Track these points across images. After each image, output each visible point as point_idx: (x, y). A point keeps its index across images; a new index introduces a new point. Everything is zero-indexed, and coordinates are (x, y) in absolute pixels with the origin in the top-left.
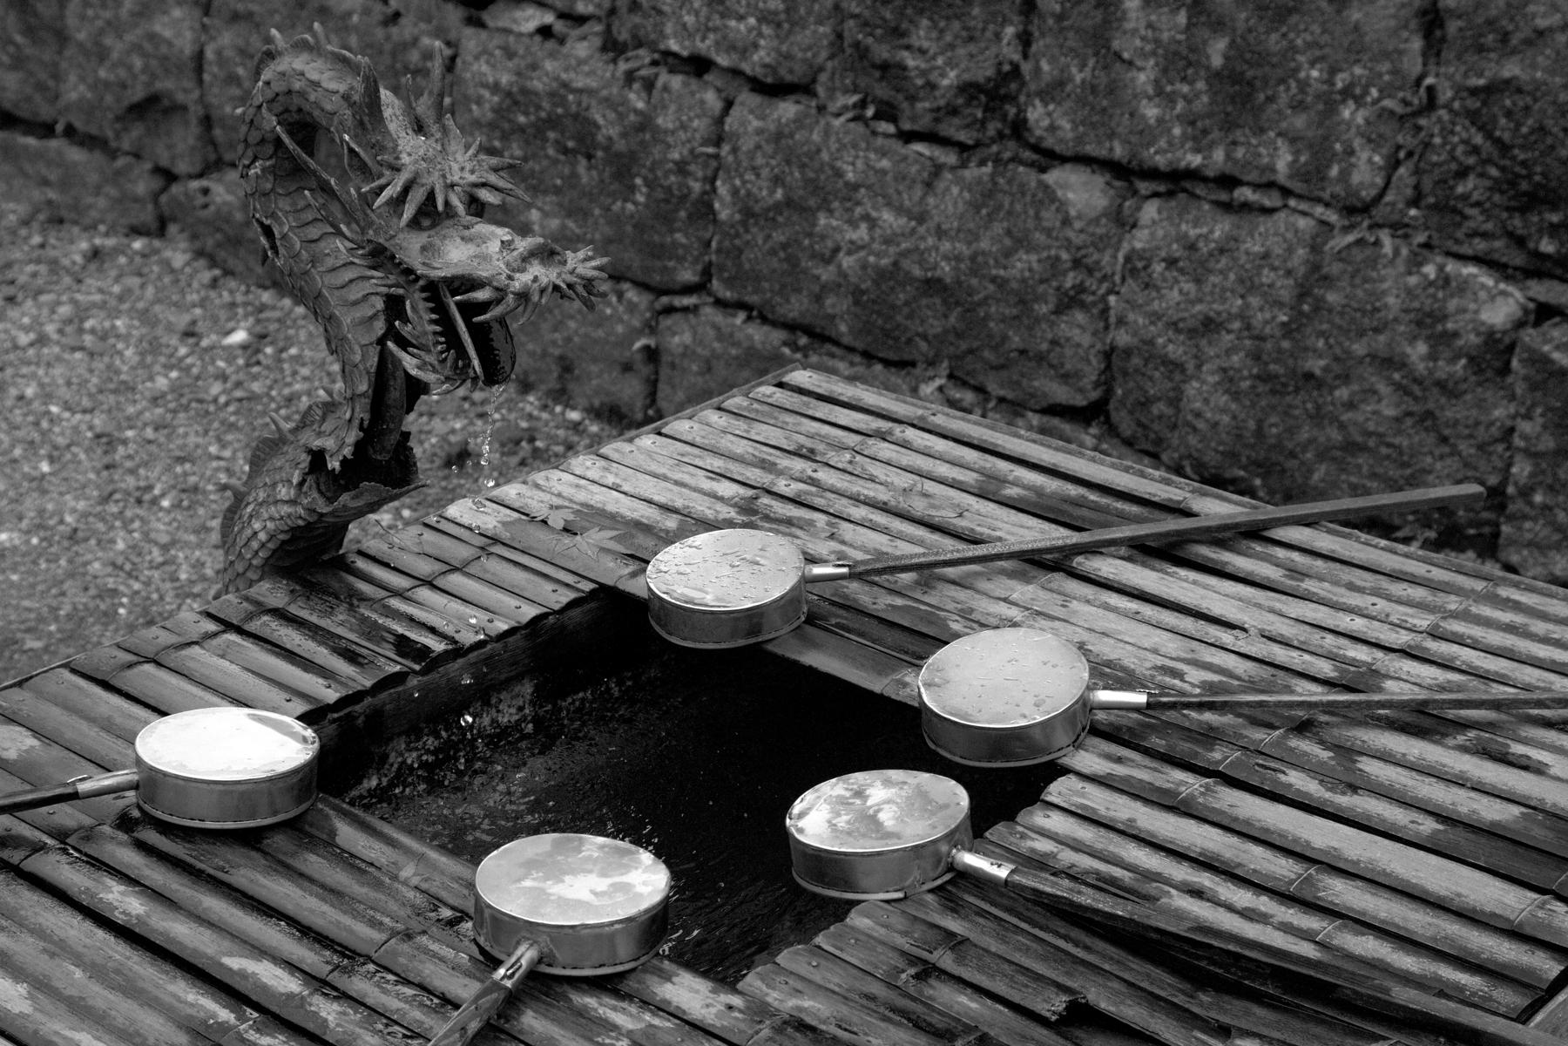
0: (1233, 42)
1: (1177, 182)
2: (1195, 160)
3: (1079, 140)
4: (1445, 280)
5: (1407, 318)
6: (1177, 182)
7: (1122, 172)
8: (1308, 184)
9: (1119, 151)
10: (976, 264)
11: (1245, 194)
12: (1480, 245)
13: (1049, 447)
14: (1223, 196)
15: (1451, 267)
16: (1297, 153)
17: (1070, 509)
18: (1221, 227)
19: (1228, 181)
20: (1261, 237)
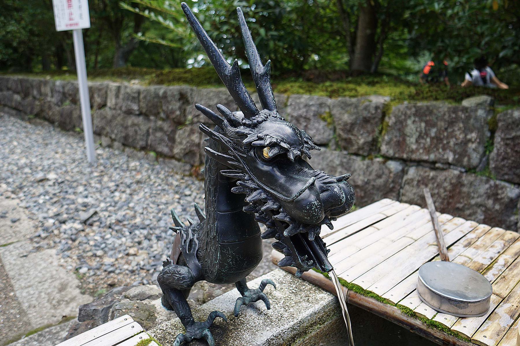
0: (438, 130)
1: (419, 163)
2: (425, 157)
3: (394, 154)
4: (496, 186)
5: (150, 171)
6: (419, 163)
7: (405, 162)
8: (457, 163)
9: (405, 156)
10: (367, 183)
11: (437, 165)
12: (506, 177)
13: (378, 298)
14: (432, 166)
15: (498, 182)
16: (455, 156)
17: (376, 80)
18: (432, 174)
19: (434, 163)
20: (442, 176)
